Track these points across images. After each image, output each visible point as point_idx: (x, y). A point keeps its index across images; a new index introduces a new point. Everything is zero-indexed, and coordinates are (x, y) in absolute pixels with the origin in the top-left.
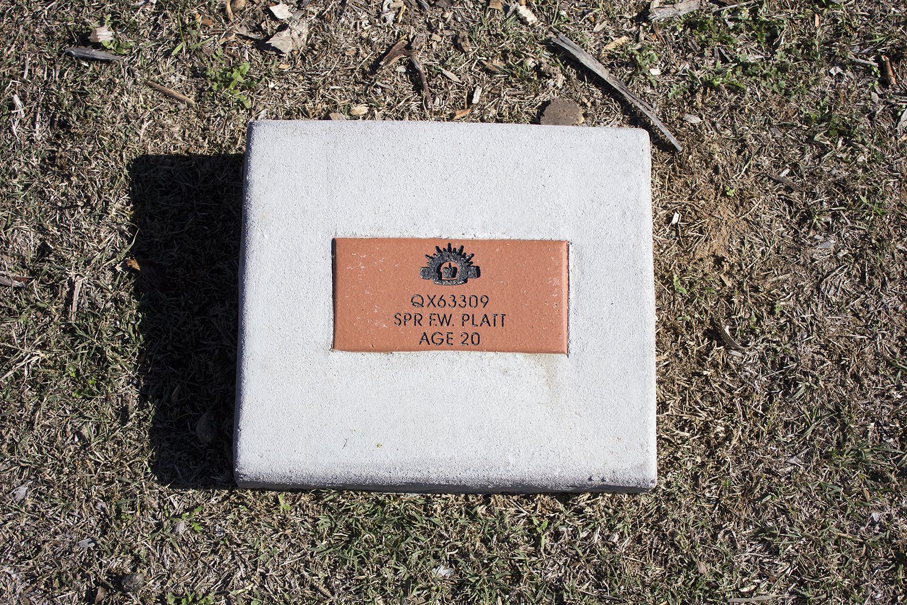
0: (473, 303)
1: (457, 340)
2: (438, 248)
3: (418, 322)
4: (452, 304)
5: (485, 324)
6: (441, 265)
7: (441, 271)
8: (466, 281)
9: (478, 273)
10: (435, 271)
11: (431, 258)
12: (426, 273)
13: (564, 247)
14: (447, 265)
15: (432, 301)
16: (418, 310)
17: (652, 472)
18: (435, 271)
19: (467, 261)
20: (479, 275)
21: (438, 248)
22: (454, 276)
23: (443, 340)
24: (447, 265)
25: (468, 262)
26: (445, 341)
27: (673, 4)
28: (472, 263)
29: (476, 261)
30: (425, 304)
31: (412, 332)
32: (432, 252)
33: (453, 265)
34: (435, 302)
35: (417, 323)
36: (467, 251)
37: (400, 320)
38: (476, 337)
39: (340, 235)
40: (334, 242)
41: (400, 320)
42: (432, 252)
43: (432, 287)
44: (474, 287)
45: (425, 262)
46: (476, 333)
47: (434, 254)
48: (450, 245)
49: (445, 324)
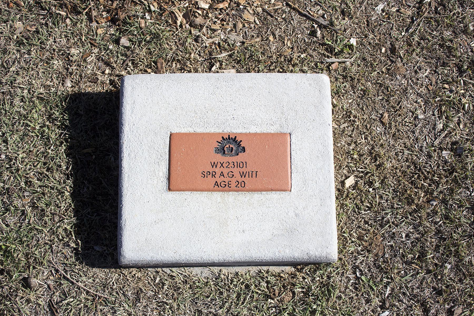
1: (233, 185)
2: (223, 137)
3: (213, 176)
5: (216, 186)
7: (225, 149)
8: (238, 154)
9: (244, 150)
10: (221, 150)
11: (220, 143)
15: (222, 165)
17: (334, 254)
18: (221, 150)
19: (238, 144)
20: (244, 151)
21: (223, 137)
22: (232, 152)
23: (226, 185)
24: (227, 146)
25: (239, 145)
26: (227, 186)
28: (241, 145)
29: (243, 144)
31: (211, 181)
32: (220, 139)
33: (231, 146)
34: (219, 165)
36: (238, 139)
39: (173, 132)
40: (171, 135)
43: (219, 158)
44: (241, 157)
45: (216, 145)
47: (221, 141)
48: (229, 136)
49: (243, 176)
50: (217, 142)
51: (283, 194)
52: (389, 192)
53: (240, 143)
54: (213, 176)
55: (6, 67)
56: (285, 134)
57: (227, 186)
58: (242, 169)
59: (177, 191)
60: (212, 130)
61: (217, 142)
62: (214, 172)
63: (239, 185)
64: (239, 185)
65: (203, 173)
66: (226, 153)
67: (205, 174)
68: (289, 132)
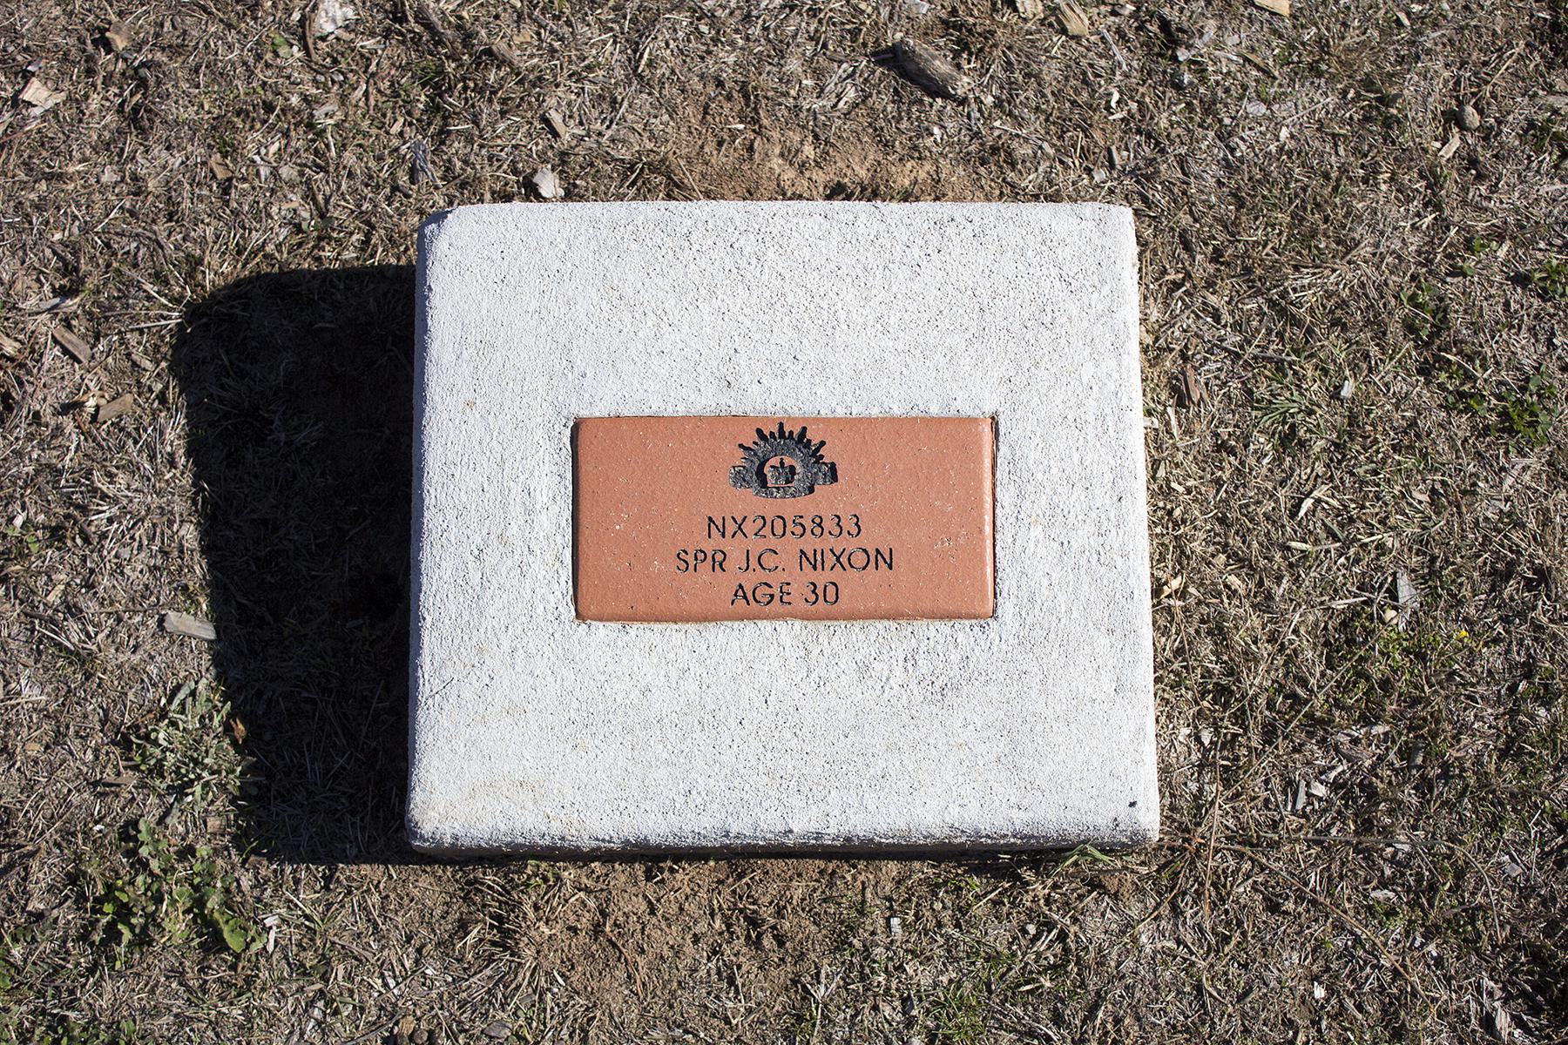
0: (779, 530)
1: (799, 590)
2: (759, 432)
3: (719, 564)
4: (836, 531)
6: (762, 465)
7: (767, 470)
8: (811, 490)
9: (833, 475)
12: (740, 479)
13: (987, 429)
14: (775, 461)
15: (740, 528)
16: (716, 542)
19: (814, 454)
20: (834, 478)
21: (759, 432)
23: (772, 596)
24: (775, 461)
26: (777, 598)
27: (578, 616)
28: (822, 457)
29: (828, 454)
30: (729, 533)
32: (750, 438)
33: (788, 461)
34: (731, 527)
35: (717, 566)
36: (814, 436)
37: (687, 561)
38: (831, 590)
41: (687, 561)
42: (750, 438)
43: (749, 502)
44: (826, 501)
46: (702, 551)
48: (781, 425)
50: (741, 446)
51: (964, 632)
52: (1544, 603)
53: (818, 450)
54: (719, 564)
55: (1302, 513)
56: (975, 420)
57: (777, 598)
58: (817, 540)
59: (658, 620)
60: (704, 400)
61: (741, 446)
62: (702, 551)
63: (767, 531)
64: (767, 531)
65: (683, 555)
66: (771, 482)
67: (690, 559)
68: (989, 409)
